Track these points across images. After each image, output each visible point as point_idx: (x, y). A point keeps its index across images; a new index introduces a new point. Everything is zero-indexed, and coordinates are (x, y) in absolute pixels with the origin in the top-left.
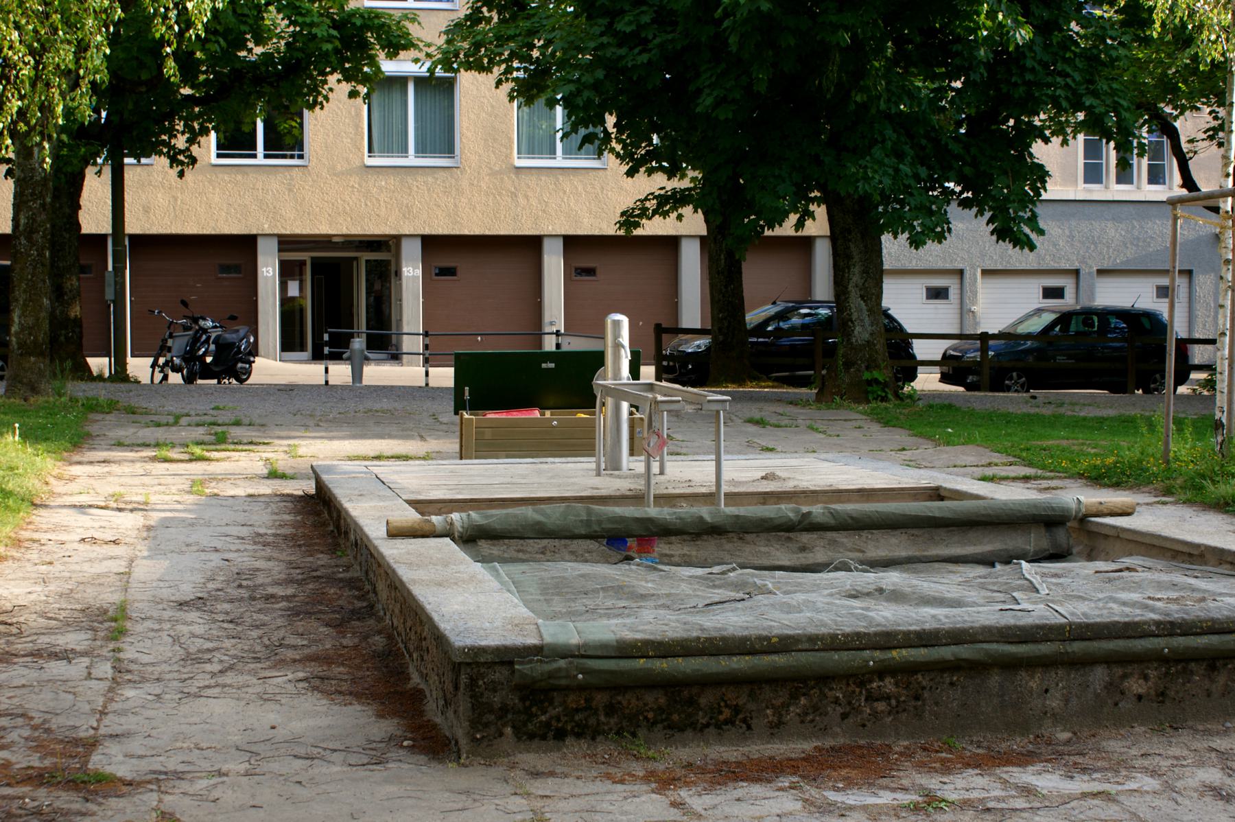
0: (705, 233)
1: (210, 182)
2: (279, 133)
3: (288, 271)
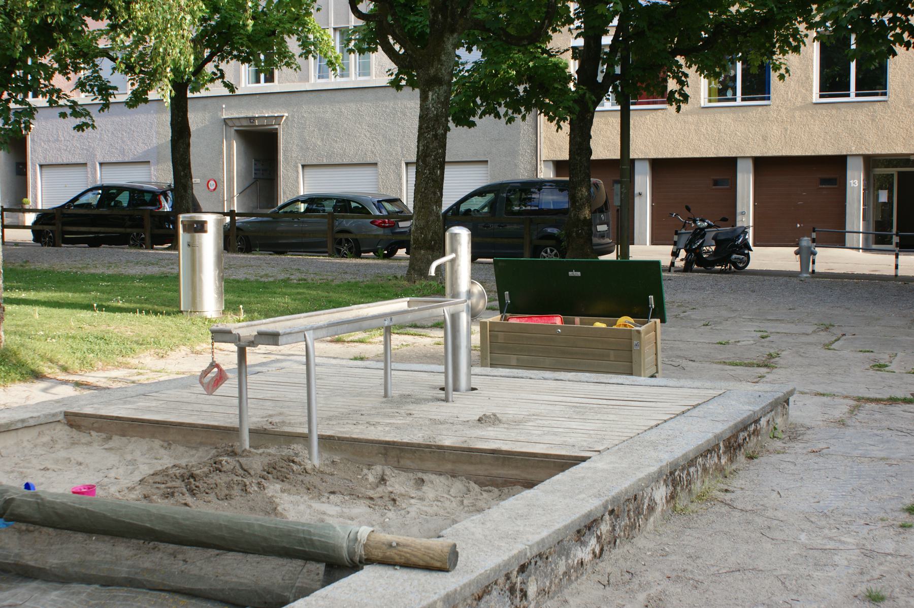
0: (565, 156)
1: (812, 116)
2: (560, 68)
3: (873, 183)
